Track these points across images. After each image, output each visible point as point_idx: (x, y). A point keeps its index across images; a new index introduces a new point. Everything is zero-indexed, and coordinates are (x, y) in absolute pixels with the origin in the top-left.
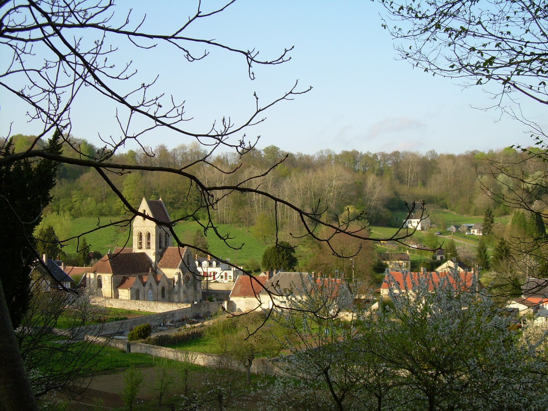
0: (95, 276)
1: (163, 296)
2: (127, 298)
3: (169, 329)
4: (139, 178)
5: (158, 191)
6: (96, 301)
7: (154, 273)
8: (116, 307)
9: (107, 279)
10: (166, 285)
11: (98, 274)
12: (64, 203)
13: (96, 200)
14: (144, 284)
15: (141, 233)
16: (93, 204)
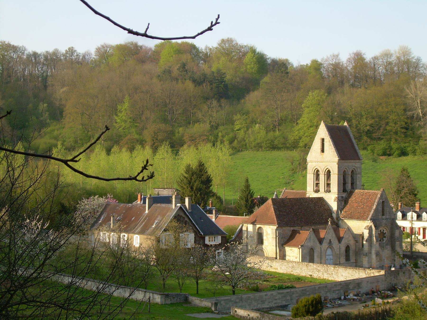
0: (254, 229)
1: (348, 259)
2: (297, 260)
3: (352, 304)
4: (324, 97)
5: (350, 115)
6: (252, 261)
7: (335, 226)
8: (281, 272)
9: (270, 232)
10: (352, 243)
11: (258, 226)
12: (224, 132)
13: (266, 128)
14: (321, 241)
15: (318, 171)
16: (263, 133)
